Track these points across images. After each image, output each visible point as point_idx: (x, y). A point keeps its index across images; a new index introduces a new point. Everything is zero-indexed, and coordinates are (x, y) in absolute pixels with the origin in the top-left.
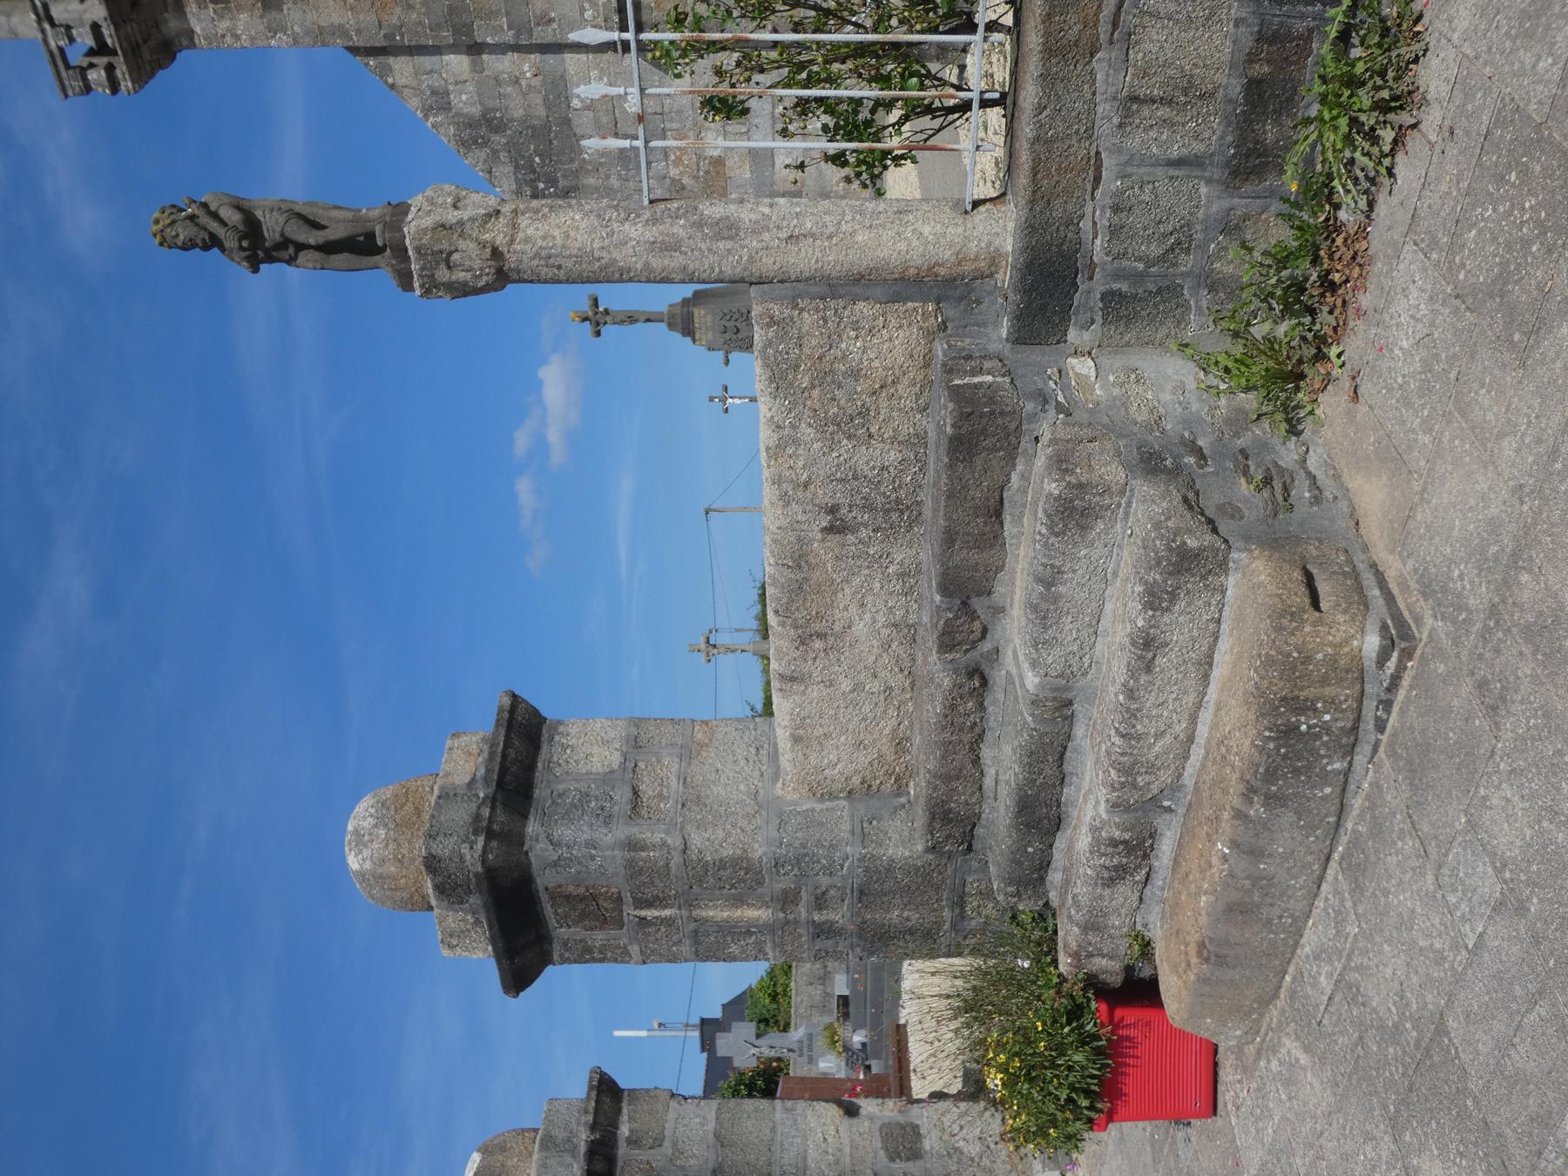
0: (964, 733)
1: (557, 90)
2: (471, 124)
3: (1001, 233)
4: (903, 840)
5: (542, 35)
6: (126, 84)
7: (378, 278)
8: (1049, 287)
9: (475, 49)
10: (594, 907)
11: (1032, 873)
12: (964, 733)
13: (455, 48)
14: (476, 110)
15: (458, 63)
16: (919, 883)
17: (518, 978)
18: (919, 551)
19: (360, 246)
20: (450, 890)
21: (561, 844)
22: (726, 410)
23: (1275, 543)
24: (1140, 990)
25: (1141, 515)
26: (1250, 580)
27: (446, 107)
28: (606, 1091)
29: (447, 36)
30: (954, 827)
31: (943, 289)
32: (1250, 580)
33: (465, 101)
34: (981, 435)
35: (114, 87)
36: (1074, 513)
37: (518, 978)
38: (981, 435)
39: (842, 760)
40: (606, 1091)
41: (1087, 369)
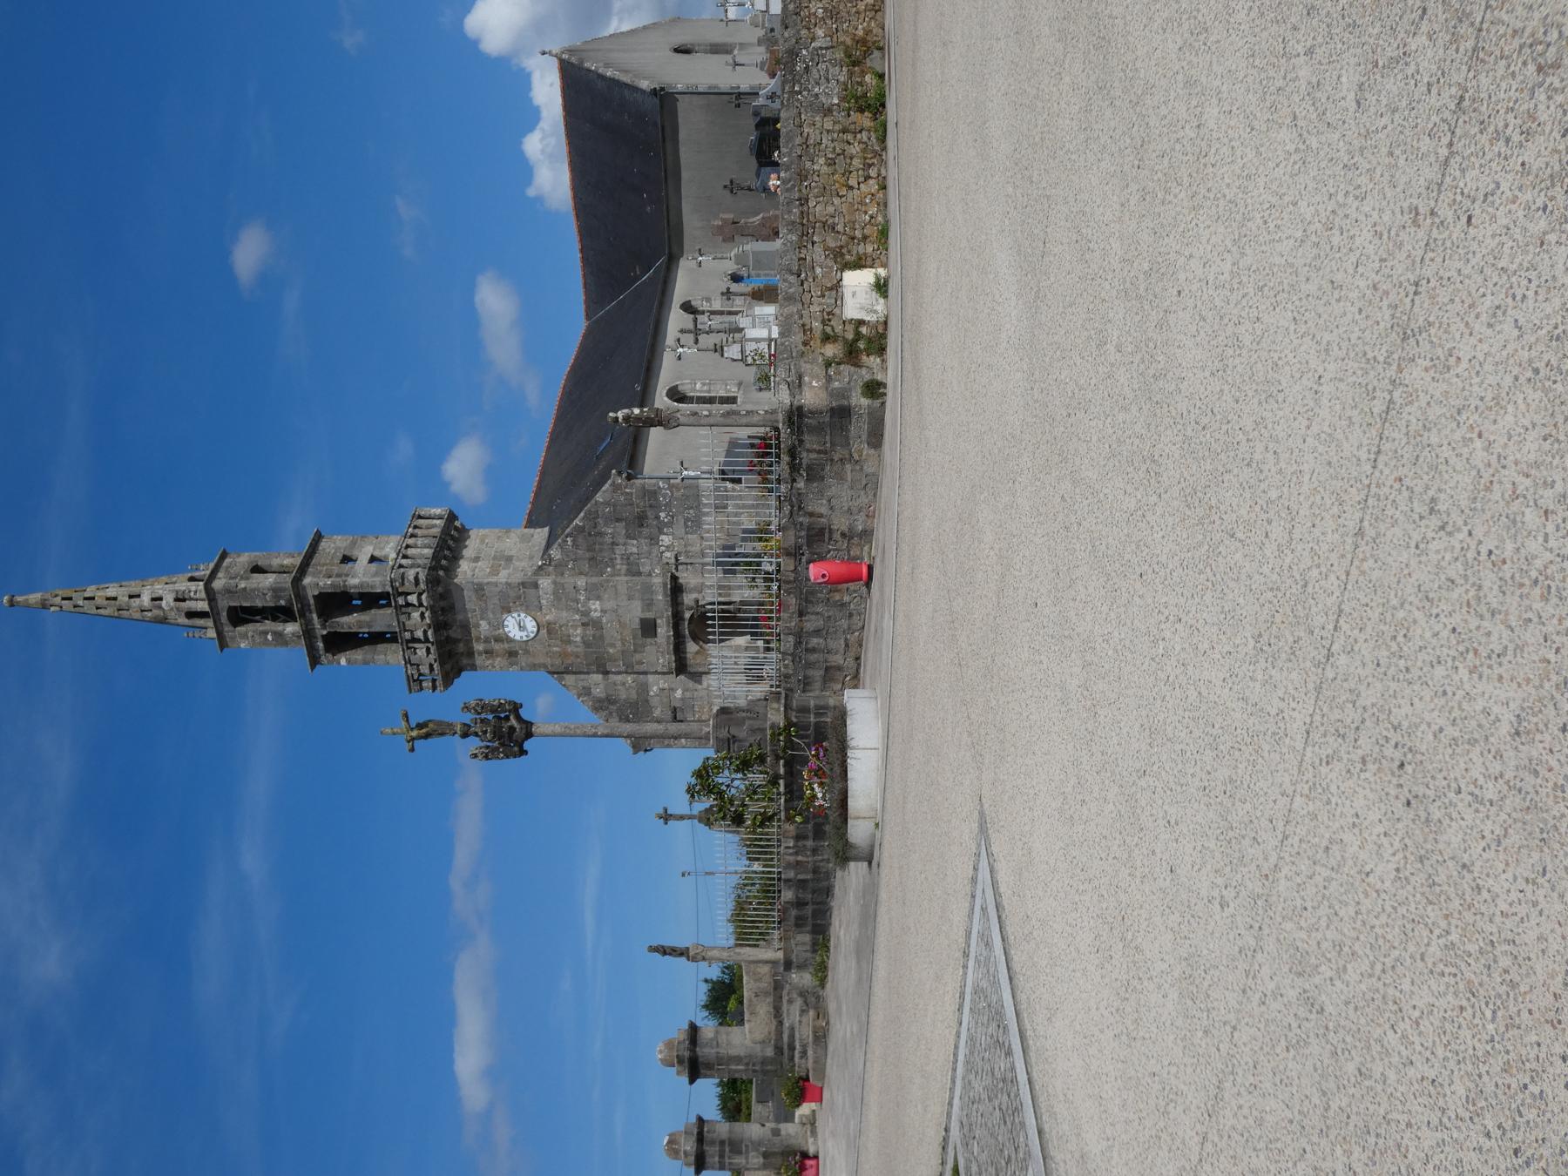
0: (779, 1033)
1: (643, 689)
2: (600, 701)
3: (780, 955)
4: (770, 1052)
5: (637, 668)
6: (440, 687)
7: (683, 959)
8: (788, 965)
9: (606, 673)
10: (709, 1066)
11: (792, 1058)
12: (779, 1033)
13: (597, 672)
14: (603, 695)
15: (598, 677)
16: (772, 1061)
17: (692, 1081)
18: (770, 999)
19: (681, 954)
20: (680, 1061)
21: (705, 1052)
22: (679, 358)
23: (816, 1008)
24: (807, 1079)
25: (799, 1002)
26: (812, 1013)
27: (589, 694)
28: (700, 1120)
29: (594, 668)
30: (779, 1049)
31: (774, 963)
32: (812, 1013)
33: (598, 692)
34: (778, 987)
35: (434, 688)
36: (790, 1002)
37: (692, 1081)
38: (778, 987)
39: (759, 1036)
40: (700, 1120)
41: (794, 976)
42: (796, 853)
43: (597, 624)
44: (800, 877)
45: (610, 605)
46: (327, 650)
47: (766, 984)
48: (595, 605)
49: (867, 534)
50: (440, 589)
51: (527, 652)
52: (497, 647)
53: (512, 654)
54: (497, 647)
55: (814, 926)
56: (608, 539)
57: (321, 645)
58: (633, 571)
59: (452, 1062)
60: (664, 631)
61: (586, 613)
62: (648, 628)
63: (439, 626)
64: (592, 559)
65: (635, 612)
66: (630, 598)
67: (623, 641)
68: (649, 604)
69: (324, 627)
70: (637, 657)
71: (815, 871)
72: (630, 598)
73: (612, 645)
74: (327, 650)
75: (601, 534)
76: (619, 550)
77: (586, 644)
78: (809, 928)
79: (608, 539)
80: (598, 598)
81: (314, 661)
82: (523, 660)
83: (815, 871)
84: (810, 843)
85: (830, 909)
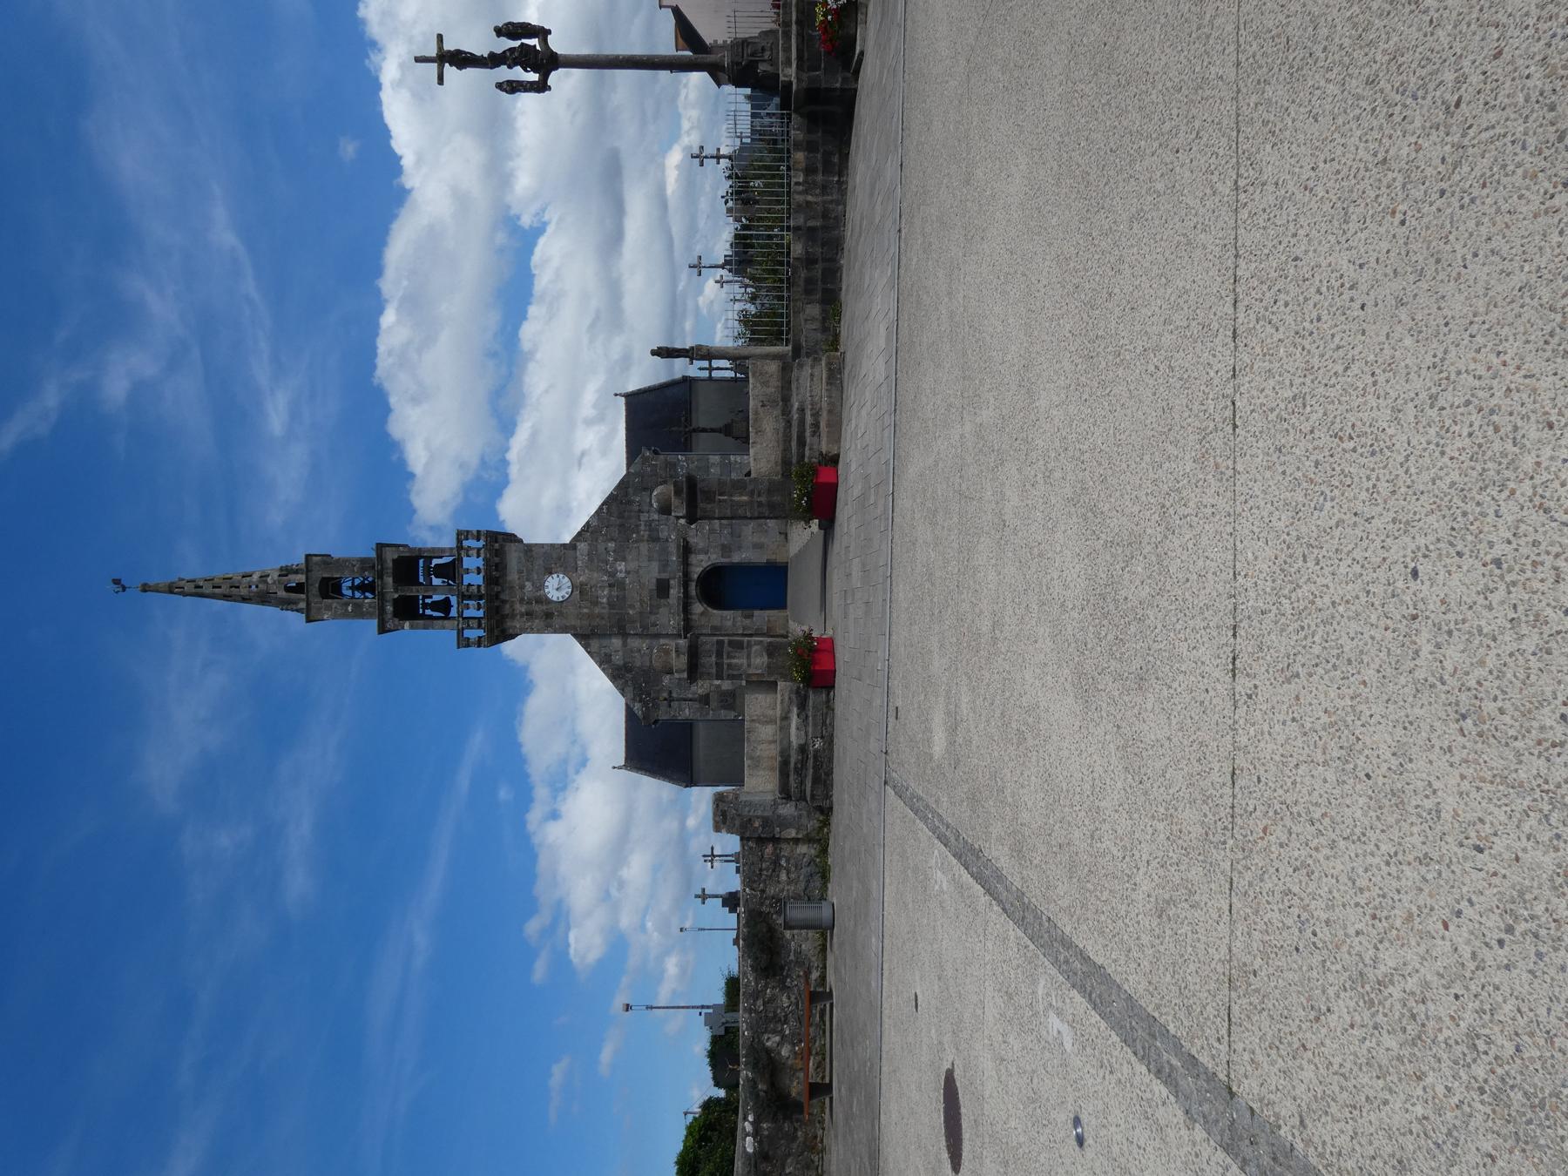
5: (653, 630)
18: (777, 412)
42: (806, 192)
43: (620, 585)
44: (811, 224)
45: (633, 566)
46: (396, 614)
47: (773, 388)
48: (621, 566)
49: (835, 460)
50: (497, 546)
51: (561, 614)
52: (537, 608)
53: (549, 615)
54: (537, 608)
55: (825, 291)
56: (635, 507)
57: (389, 608)
58: (654, 539)
59: (380, 115)
60: (675, 592)
61: (612, 574)
62: (662, 588)
63: (491, 580)
64: (622, 525)
65: (652, 573)
66: (650, 559)
67: (641, 601)
68: (664, 565)
69: (396, 591)
70: (653, 618)
71: (825, 215)
72: (650, 559)
73: (632, 607)
74: (396, 614)
75: (630, 502)
76: (644, 517)
77: (611, 605)
78: (818, 296)
79: (635, 507)
80: (624, 559)
81: (382, 629)
82: (556, 622)
83: (825, 215)
84: (820, 178)
85: (840, 268)
